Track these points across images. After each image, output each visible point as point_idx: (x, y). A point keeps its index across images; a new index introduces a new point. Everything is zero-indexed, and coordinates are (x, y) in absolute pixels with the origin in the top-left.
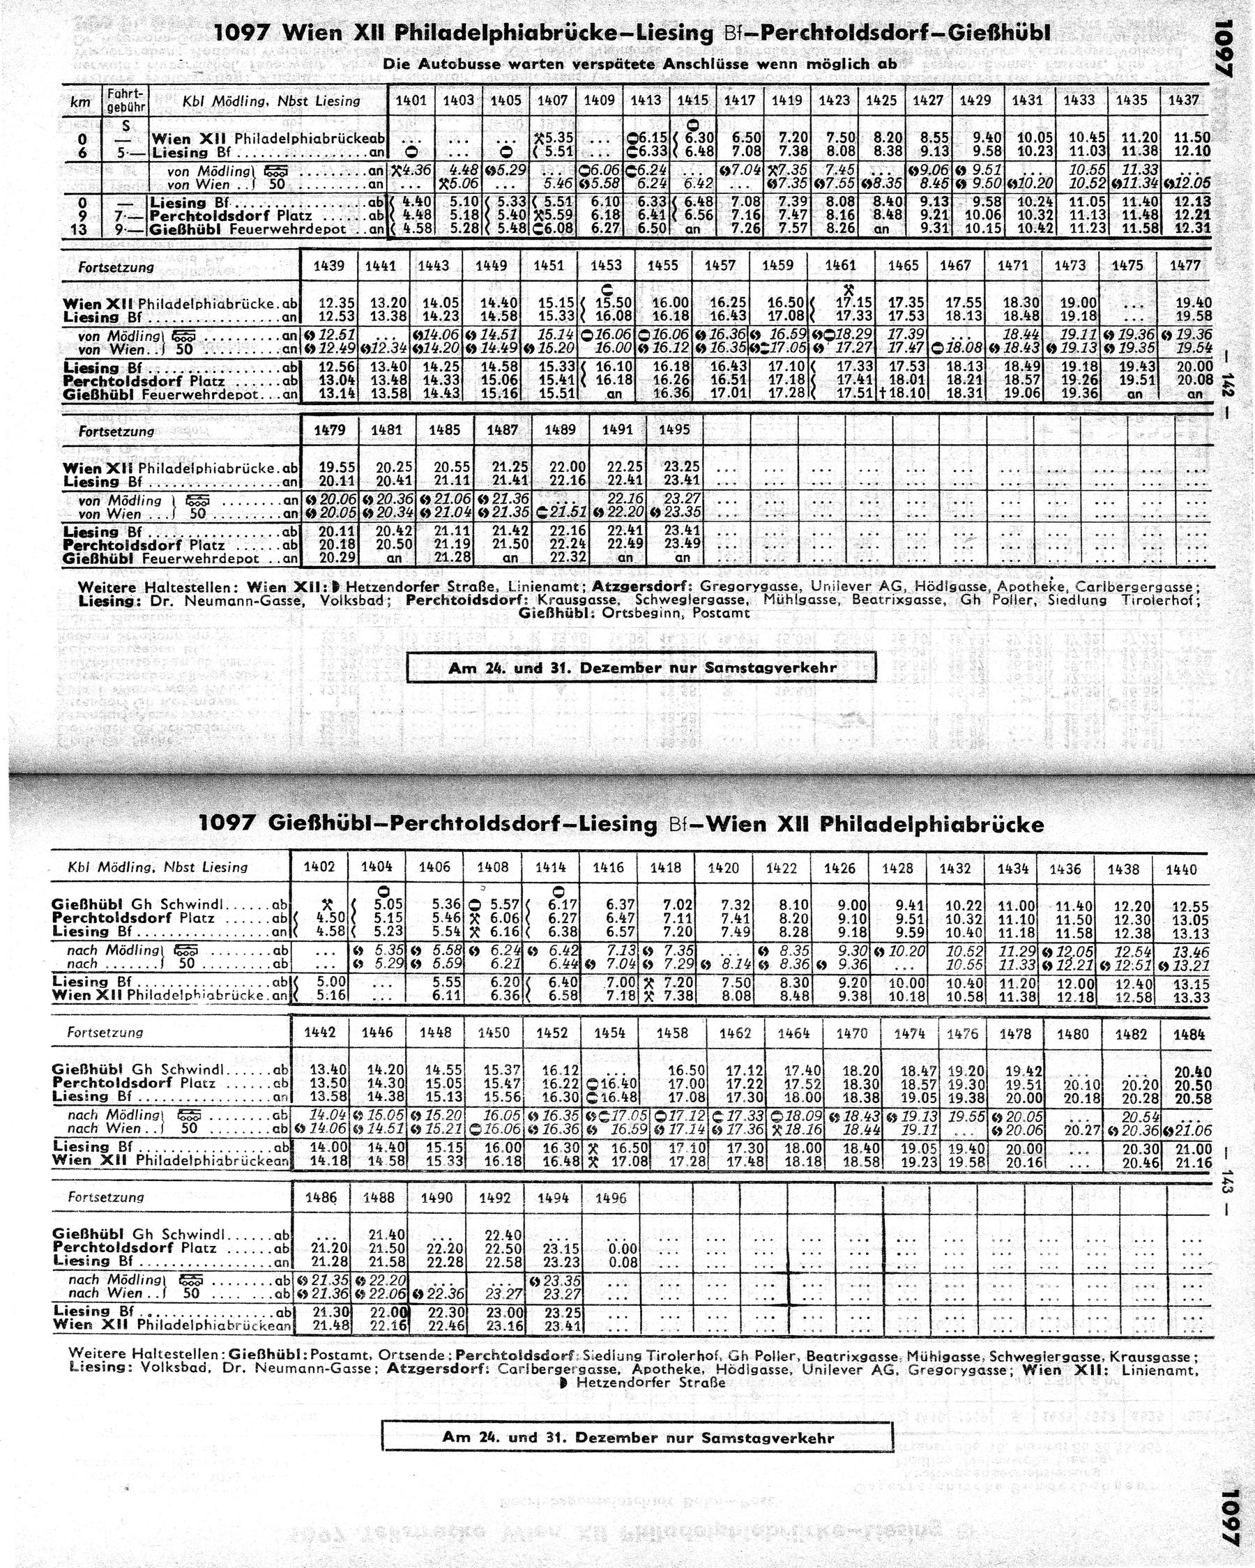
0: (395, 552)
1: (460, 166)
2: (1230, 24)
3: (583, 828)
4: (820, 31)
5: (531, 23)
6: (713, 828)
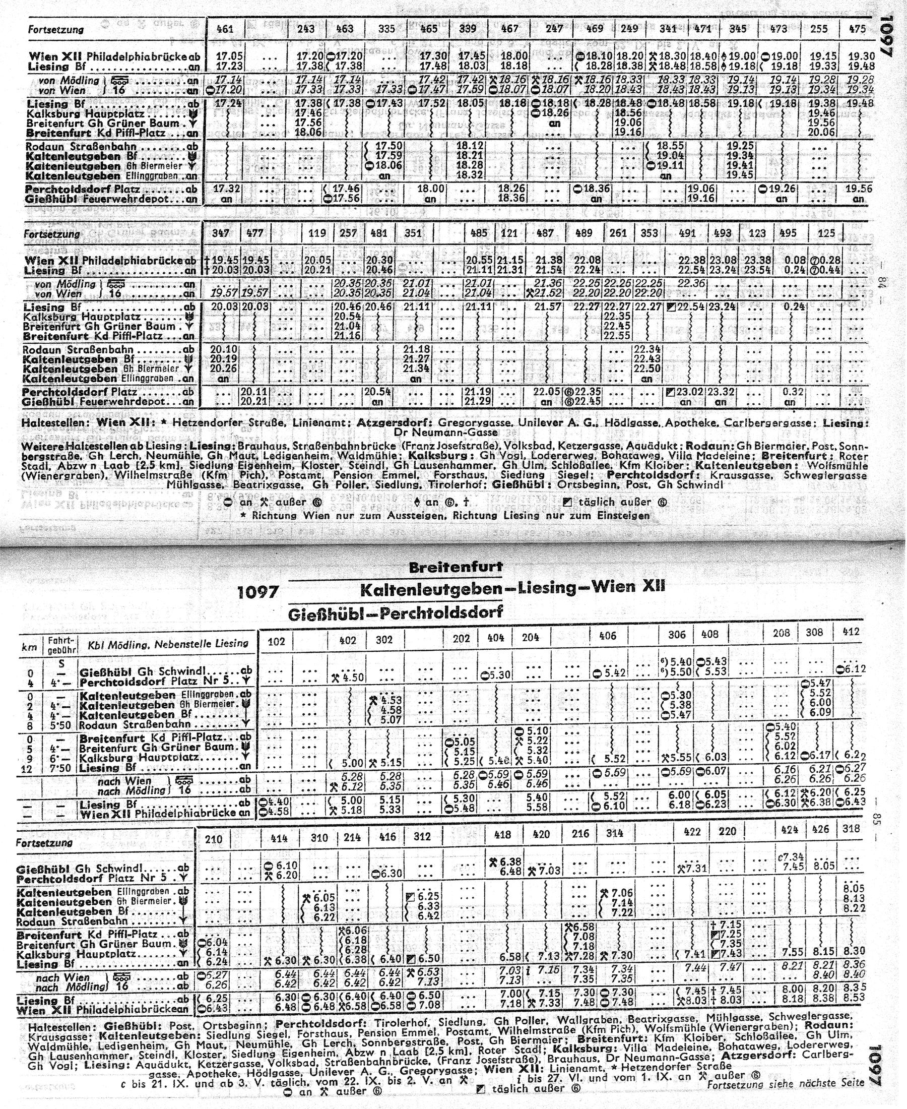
0: (378, 398)
2: (891, 18)
3: (521, 591)
4: (423, 612)
6: (597, 590)
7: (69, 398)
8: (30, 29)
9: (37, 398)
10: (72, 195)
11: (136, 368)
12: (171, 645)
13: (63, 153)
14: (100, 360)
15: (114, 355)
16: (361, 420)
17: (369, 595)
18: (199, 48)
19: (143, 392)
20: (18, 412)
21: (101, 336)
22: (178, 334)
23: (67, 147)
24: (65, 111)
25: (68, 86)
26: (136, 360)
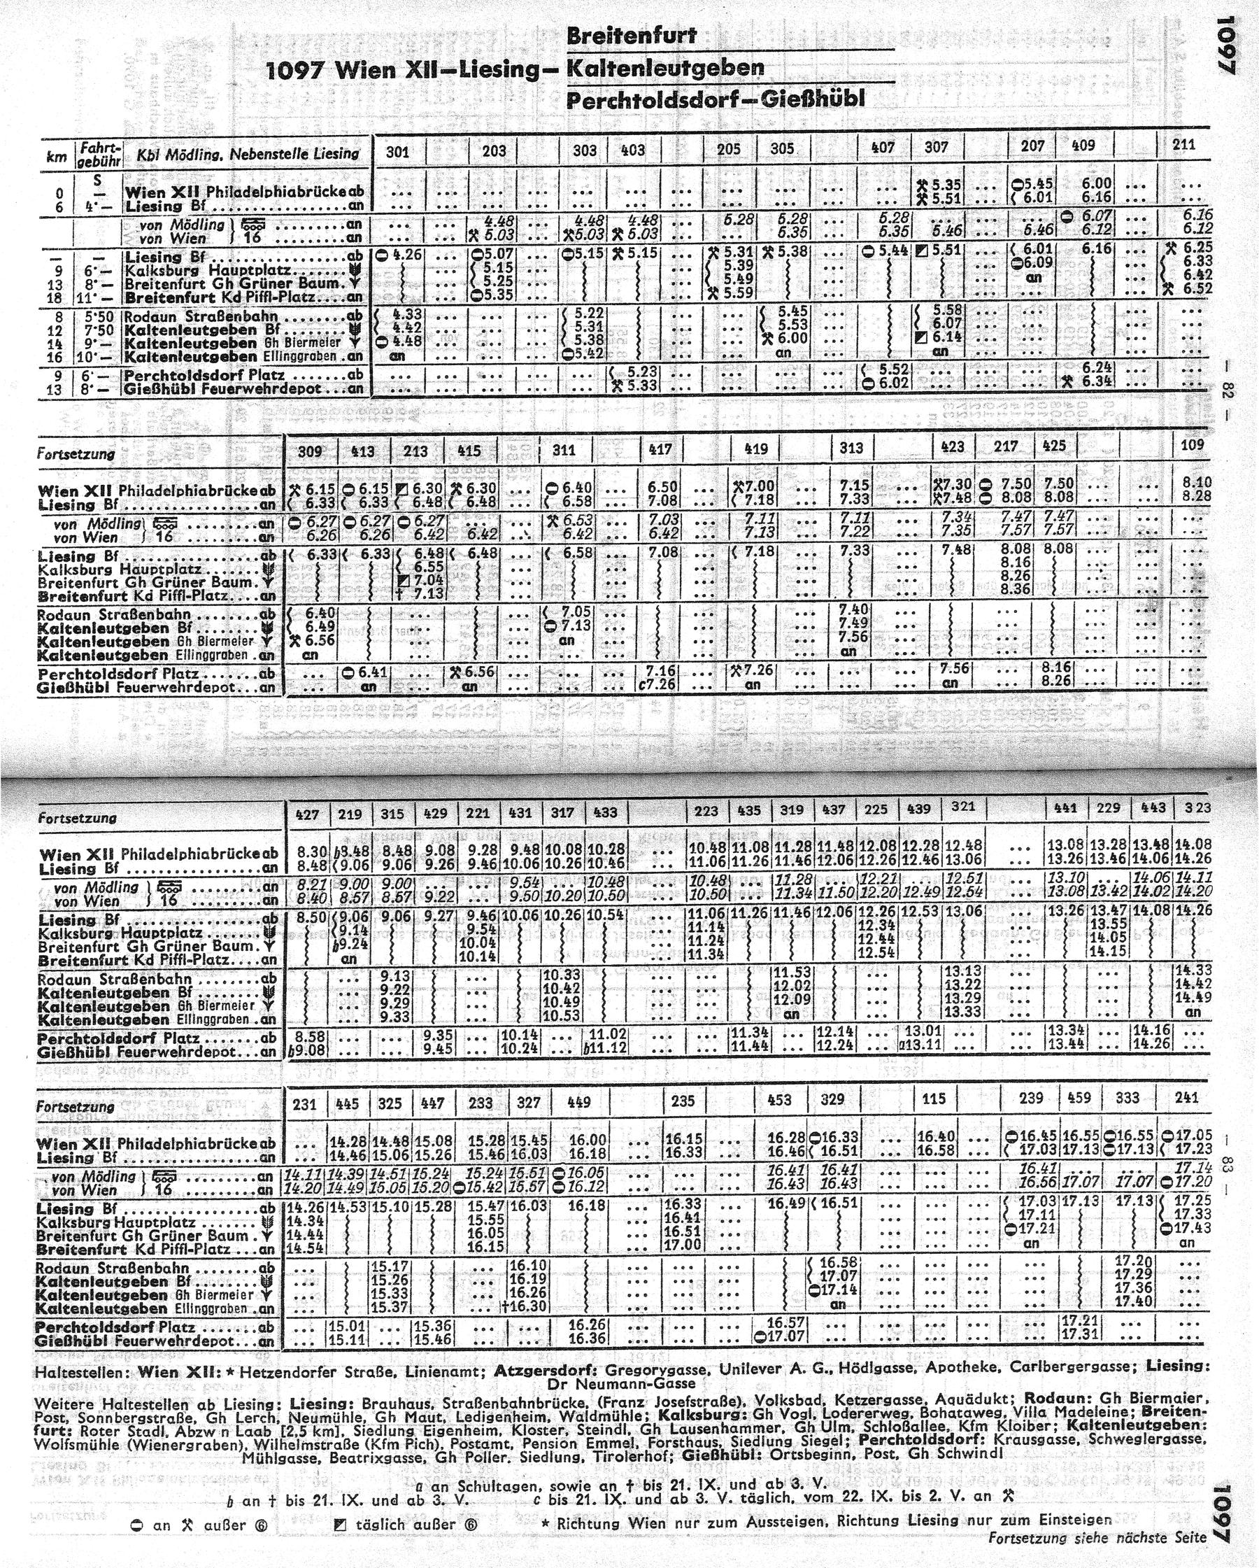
1: (585, 218)
3: (464, 75)
4: (628, 99)
5: (495, 60)
7: (103, 1047)
8: (39, 1106)
9: (58, 1047)
10: (100, 1335)
11: (195, 1005)
12: (252, 155)
13: (88, 1277)
14: (145, 628)
15: (165, 986)
16: (501, 1367)
17: (579, 74)
18: (277, 842)
19: (203, 1327)
20: (25, 1354)
21: (145, 1249)
22: (254, 957)
23: (94, 1270)
24: (92, 565)
25: (95, 894)
26: (193, 1283)
